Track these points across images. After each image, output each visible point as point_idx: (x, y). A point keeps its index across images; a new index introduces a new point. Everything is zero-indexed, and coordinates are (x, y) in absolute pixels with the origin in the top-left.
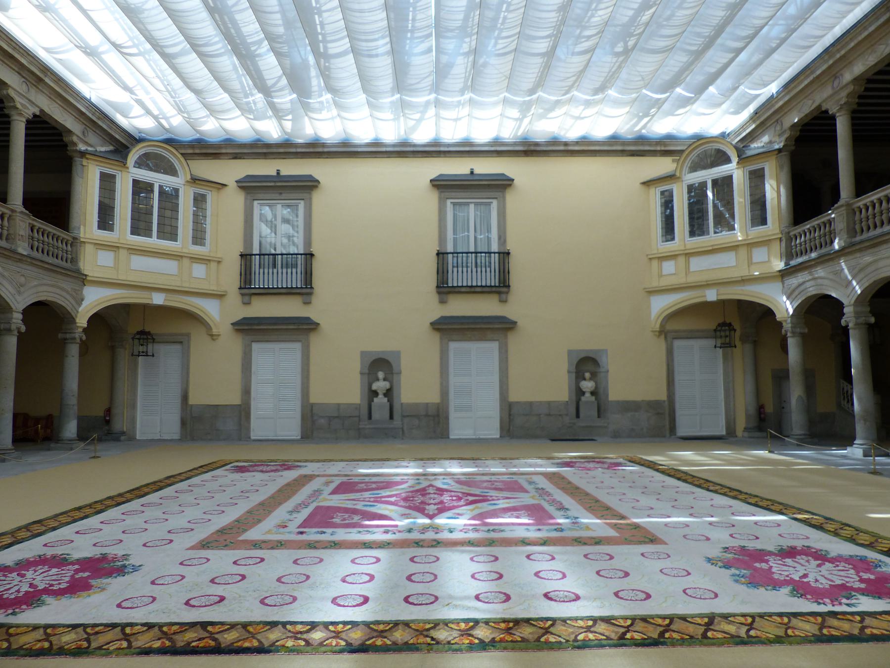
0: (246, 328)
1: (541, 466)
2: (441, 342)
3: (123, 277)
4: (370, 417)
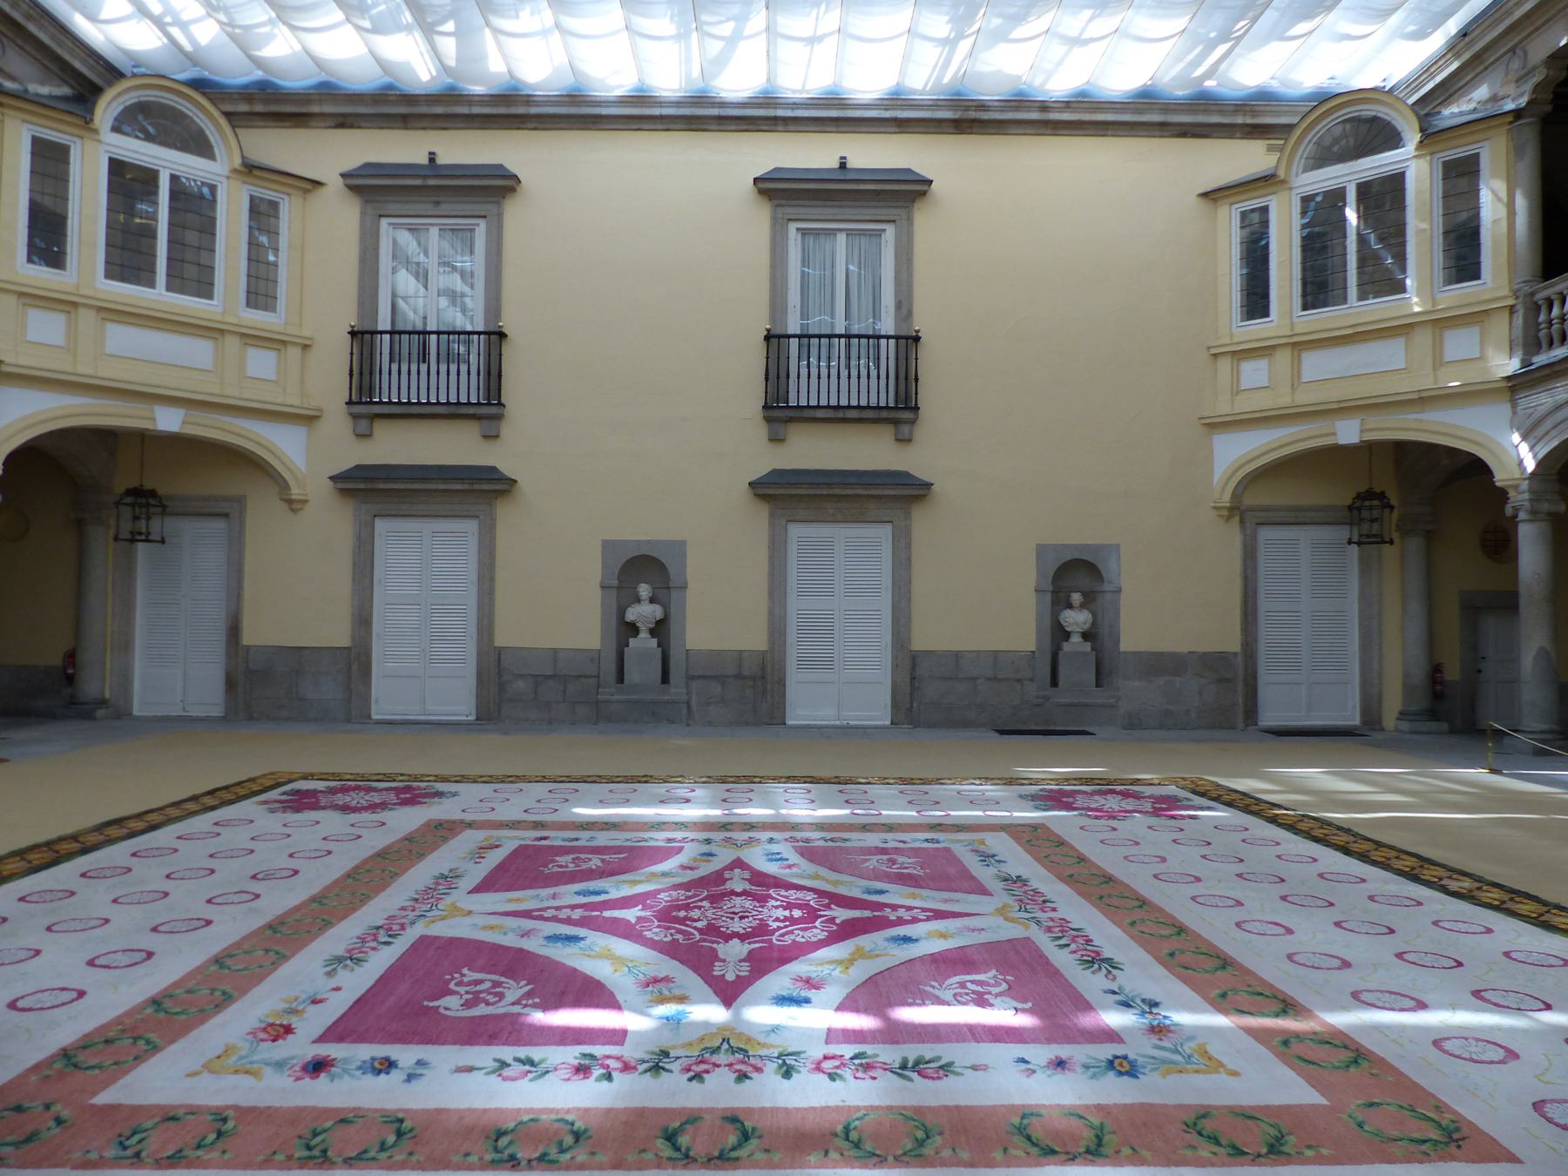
0: (362, 486)
1: (997, 803)
2: (772, 525)
3: (85, 367)
4: (620, 678)
